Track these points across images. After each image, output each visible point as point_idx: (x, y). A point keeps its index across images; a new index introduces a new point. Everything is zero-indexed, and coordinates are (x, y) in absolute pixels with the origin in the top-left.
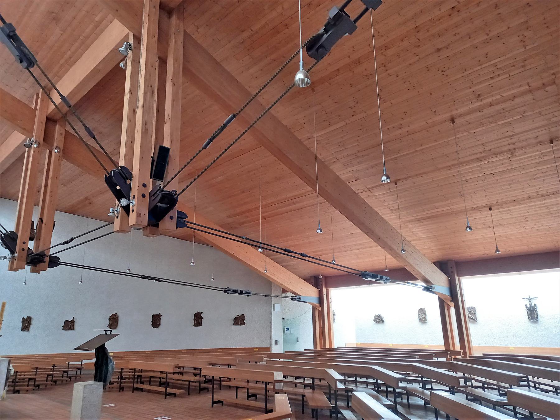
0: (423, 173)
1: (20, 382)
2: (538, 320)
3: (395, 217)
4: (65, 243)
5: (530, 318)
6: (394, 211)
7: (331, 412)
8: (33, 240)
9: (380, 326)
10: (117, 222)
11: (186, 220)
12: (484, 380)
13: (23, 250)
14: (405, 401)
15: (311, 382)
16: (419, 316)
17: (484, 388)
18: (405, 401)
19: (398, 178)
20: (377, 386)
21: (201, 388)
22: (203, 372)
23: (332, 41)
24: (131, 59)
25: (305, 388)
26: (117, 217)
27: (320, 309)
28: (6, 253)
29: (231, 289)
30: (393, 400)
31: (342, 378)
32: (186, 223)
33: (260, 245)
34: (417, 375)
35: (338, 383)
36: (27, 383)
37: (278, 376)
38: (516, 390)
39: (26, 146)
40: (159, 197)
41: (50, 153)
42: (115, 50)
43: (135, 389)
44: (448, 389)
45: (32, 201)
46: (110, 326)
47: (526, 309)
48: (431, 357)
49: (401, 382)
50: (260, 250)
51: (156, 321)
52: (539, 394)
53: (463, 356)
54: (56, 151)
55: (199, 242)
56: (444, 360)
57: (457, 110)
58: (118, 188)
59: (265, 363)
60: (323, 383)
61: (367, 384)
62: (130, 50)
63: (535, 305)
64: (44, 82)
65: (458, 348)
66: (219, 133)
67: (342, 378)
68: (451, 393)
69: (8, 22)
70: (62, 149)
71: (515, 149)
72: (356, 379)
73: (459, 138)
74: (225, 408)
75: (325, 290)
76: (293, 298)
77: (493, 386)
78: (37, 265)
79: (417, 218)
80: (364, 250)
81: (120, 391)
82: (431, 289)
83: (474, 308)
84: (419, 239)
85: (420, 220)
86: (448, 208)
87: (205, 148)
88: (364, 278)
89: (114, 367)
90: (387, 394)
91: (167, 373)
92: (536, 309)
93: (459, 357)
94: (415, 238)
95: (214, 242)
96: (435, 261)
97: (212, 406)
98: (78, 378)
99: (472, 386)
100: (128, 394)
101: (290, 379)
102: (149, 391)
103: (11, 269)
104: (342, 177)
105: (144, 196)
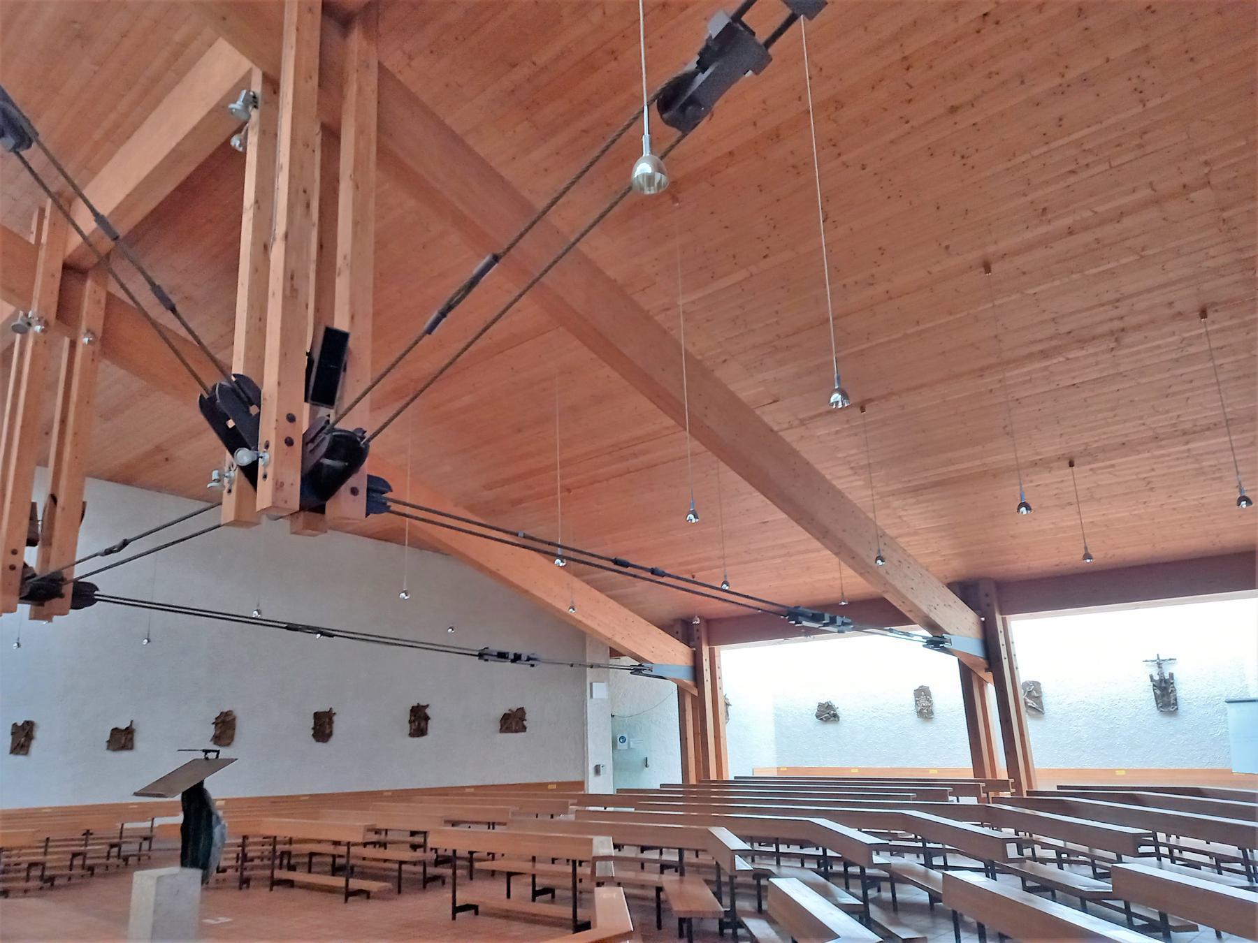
0: (922, 386)
2: (1177, 709)
4: (109, 552)
5: (1160, 705)
7: (722, 925)
9: (830, 728)
10: (229, 502)
12: (1060, 843)
14: (886, 895)
16: (916, 704)
17: (1060, 863)
22: (431, 842)
23: (719, 85)
25: (662, 872)
27: (695, 692)
30: (860, 892)
31: (747, 846)
33: (559, 551)
34: (913, 836)
37: (602, 845)
38: (1134, 865)
39: (16, 329)
41: (73, 345)
42: (220, 109)
43: (275, 883)
44: (981, 865)
46: (217, 739)
47: (1151, 684)
48: (943, 795)
50: (558, 561)
51: (323, 726)
52: (1179, 872)
53: (1013, 790)
54: (86, 340)
56: (972, 801)
57: (996, 243)
59: (572, 817)
60: (704, 859)
61: (803, 858)
62: (255, 107)
63: (1171, 675)
64: (57, 183)
65: (1002, 773)
67: (747, 846)
71: (1123, 330)
73: (1000, 306)
75: (705, 650)
76: (634, 669)
82: (943, 643)
83: (1037, 684)
84: (915, 533)
85: (916, 490)
88: (794, 622)
89: (225, 834)
90: (845, 879)
91: (348, 844)
92: (1172, 683)
93: (1007, 795)
97: (454, 918)
98: (143, 860)
100: (259, 895)
104: (744, 395)
105: (289, 442)
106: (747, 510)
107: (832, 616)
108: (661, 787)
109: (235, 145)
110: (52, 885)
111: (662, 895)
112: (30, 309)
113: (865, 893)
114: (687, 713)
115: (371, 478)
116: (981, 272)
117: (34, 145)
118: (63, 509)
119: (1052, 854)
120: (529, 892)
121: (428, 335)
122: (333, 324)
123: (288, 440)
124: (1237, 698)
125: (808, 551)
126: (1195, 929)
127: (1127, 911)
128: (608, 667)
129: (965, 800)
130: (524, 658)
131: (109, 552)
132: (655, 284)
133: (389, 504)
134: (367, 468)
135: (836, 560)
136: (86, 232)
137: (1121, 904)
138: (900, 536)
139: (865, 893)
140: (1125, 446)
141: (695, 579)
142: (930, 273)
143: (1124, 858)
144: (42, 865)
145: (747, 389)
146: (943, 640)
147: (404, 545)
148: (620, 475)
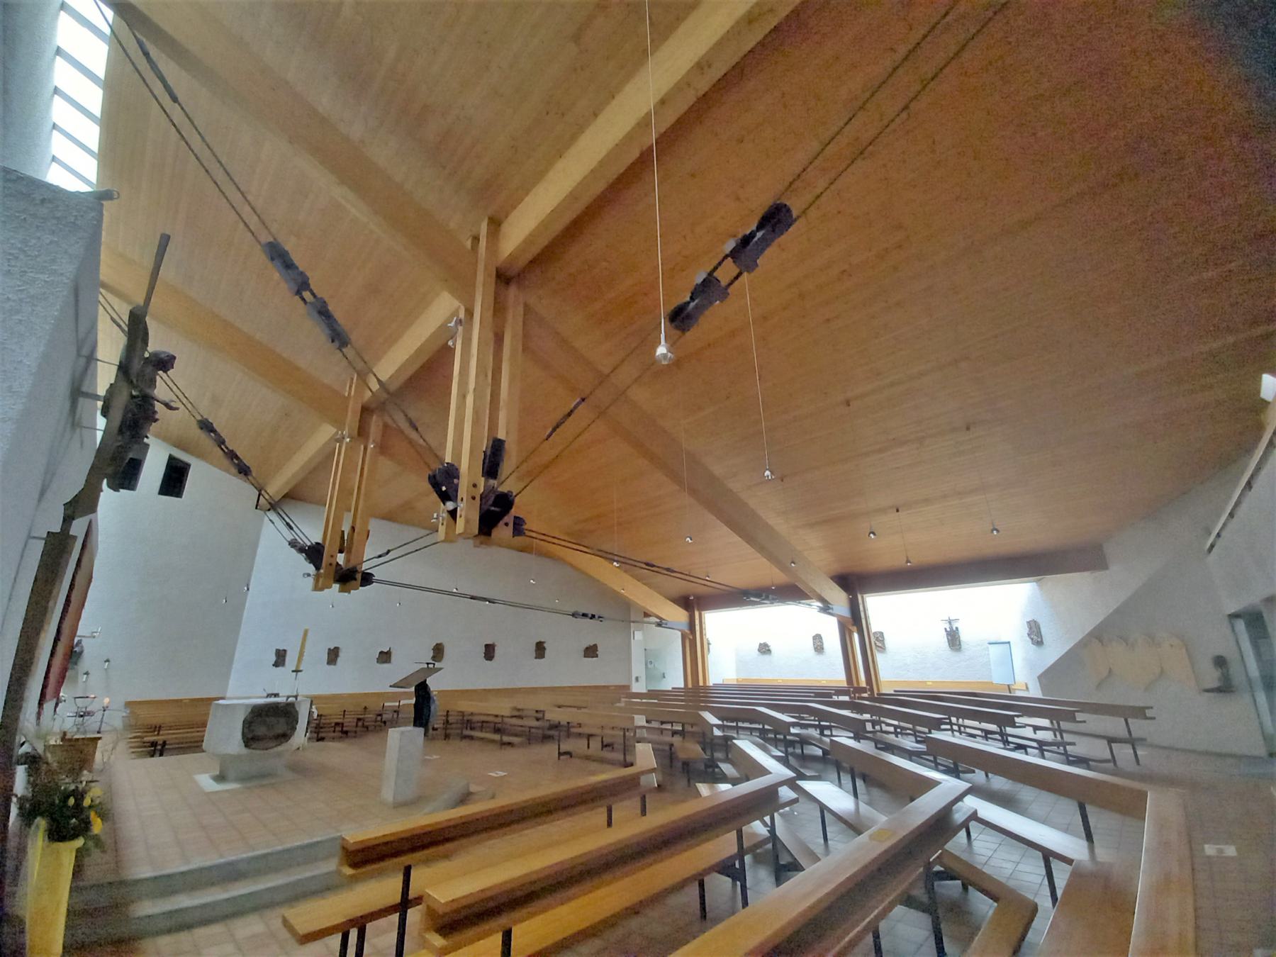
1: (325, 728)
4: (380, 556)
7: (707, 766)
9: (766, 657)
10: (442, 529)
12: (896, 723)
15: (681, 729)
17: (896, 734)
18: (798, 751)
20: (763, 733)
22: (548, 716)
23: (700, 309)
24: (461, 337)
25: (673, 736)
26: (442, 524)
27: (691, 637)
28: (311, 569)
30: (783, 749)
31: (720, 723)
33: (616, 558)
34: (813, 718)
35: (715, 729)
36: (333, 729)
37: (640, 720)
38: (936, 735)
39: (337, 440)
40: (492, 499)
41: (365, 449)
42: (444, 327)
44: (852, 735)
45: (342, 507)
46: (434, 658)
49: (793, 728)
50: (615, 563)
51: (489, 652)
52: (964, 739)
54: (372, 446)
56: (846, 698)
58: (444, 488)
59: (622, 705)
60: (695, 729)
61: (751, 730)
62: (461, 325)
63: (957, 628)
64: (360, 365)
65: (863, 683)
67: (720, 723)
68: (855, 740)
69: (319, 296)
72: (737, 724)
74: (576, 761)
75: (697, 614)
77: (908, 731)
81: (445, 739)
89: (438, 708)
90: (775, 743)
91: (503, 716)
93: (865, 695)
97: (559, 759)
98: (395, 723)
99: (882, 731)
100: (456, 744)
101: (655, 725)
102: (482, 739)
103: (317, 588)
111: (673, 749)
113: (786, 751)
115: (516, 518)
117: (349, 346)
119: (892, 729)
124: (994, 642)
126: (974, 772)
127: (935, 761)
129: (842, 698)
130: (596, 617)
131: (380, 556)
134: (514, 512)
136: (374, 390)
137: (931, 758)
139: (786, 751)
140: (927, 501)
143: (933, 731)
145: (718, 470)
147: (532, 553)
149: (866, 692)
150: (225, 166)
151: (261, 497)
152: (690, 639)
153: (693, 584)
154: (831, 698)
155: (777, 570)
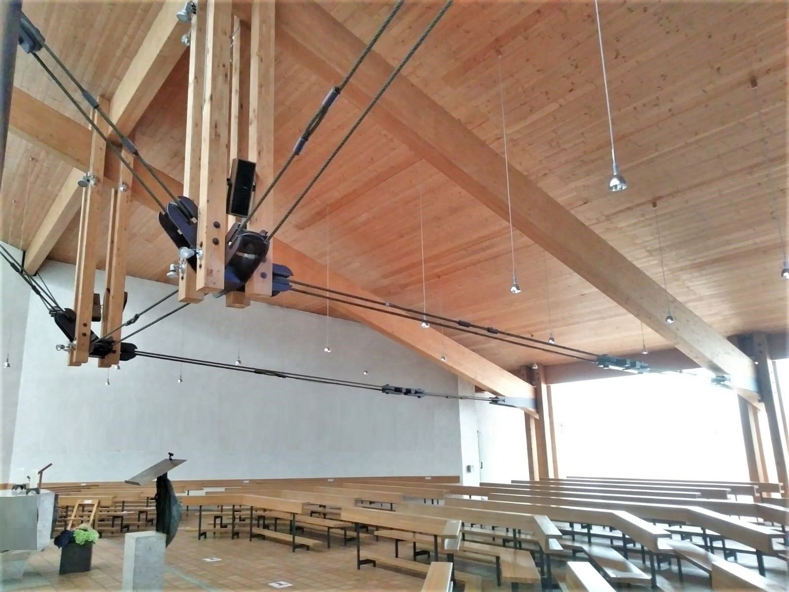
0: (702, 184)
3: (656, 262)
6: (654, 253)
8: (99, 320)
11: (290, 278)
13: (84, 335)
14: (675, 568)
18: (675, 568)
19: (658, 195)
21: (347, 537)
27: (537, 417)
28: (64, 340)
29: (393, 387)
32: (291, 284)
43: (253, 536)
44: (754, 550)
48: (723, 495)
53: (783, 492)
55: (345, 317)
57: (761, 60)
62: (195, 13)
65: (773, 479)
66: (318, 124)
70: (131, 186)
73: (766, 114)
75: (544, 387)
76: (492, 400)
78: (106, 357)
79: (695, 262)
80: (606, 320)
81: (233, 538)
82: (724, 381)
84: (701, 299)
85: (699, 267)
86: (750, 242)
87: (297, 152)
88: (602, 366)
93: (776, 496)
94: (693, 297)
95: (363, 315)
96: (729, 334)
97: (359, 568)
100: (244, 542)
104: (561, 200)
105: (216, 242)
106: (569, 286)
107: (633, 361)
108: (512, 483)
109: (184, 42)
110: (128, 529)
112: (89, 171)
114: (531, 431)
116: (748, 87)
118: (113, 297)
120: (412, 553)
121: (296, 156)
122: (248, 159)
123: (215, 240)
125: (617, 315)
128: (474, 399)
130: (413, 392)
132: (488, 120)
133: (291, 284)
135: (638, 321)
138: (689, 301)
141: (533, 338)
142: (704, 91)
144: (121, 517)
145: (562, 195)
146: (723, 379)
147: (327, 315)
148: (474, 265)
149: (778, 491)
150: (388, 26)
151: (20, 263)
152: (535, 419)
153: (549, 354)
154: (726, 498)
155: (650, 330)
